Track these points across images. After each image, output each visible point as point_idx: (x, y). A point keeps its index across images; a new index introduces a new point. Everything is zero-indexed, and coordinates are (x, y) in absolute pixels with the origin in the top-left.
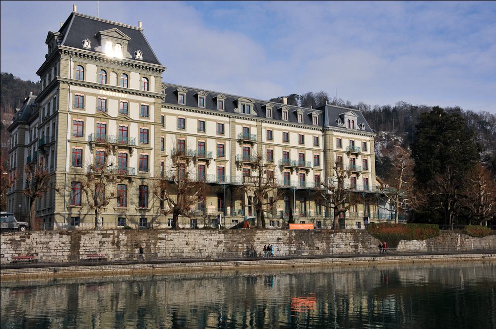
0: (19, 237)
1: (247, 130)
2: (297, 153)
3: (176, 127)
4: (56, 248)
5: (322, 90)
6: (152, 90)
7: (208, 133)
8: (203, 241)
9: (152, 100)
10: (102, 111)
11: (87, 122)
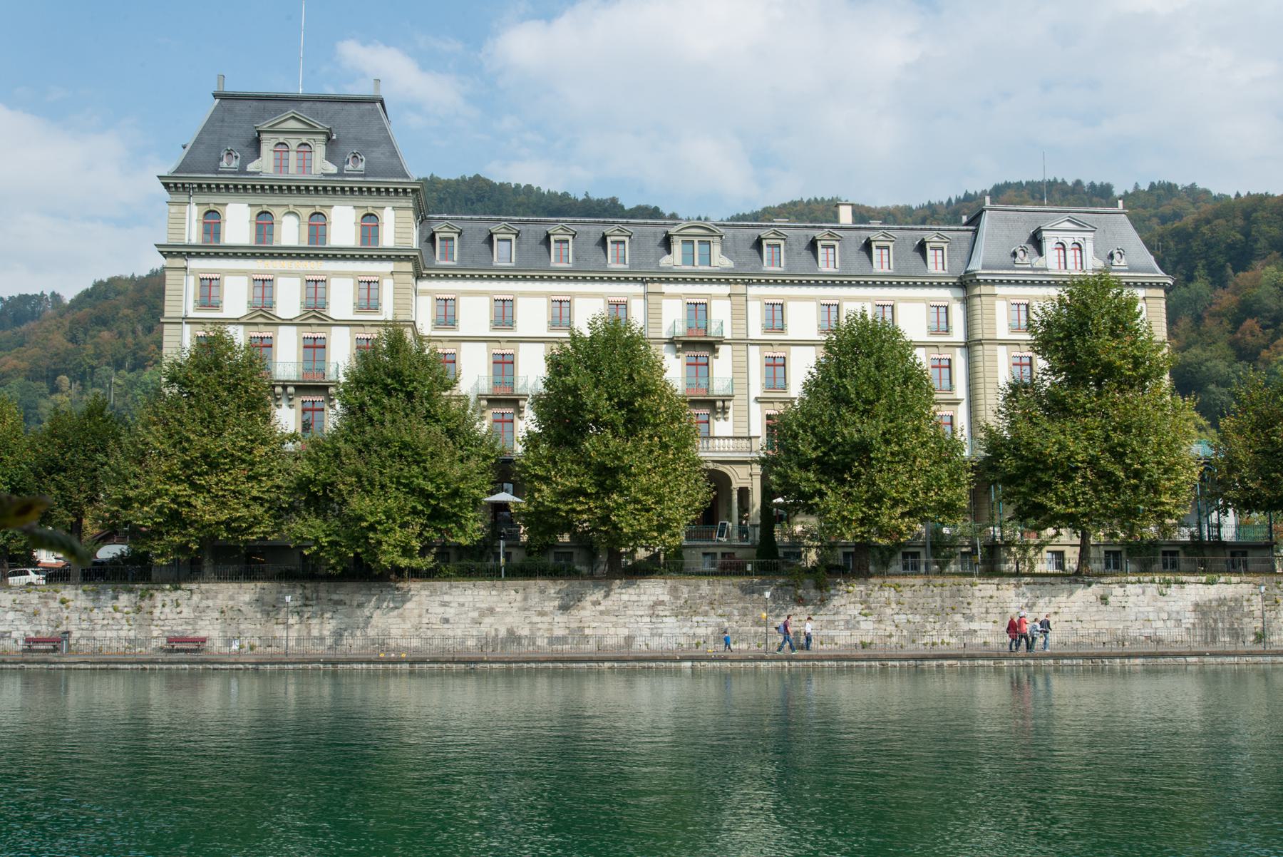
0: (37, 596)
1: (698, 309)
2: (295, 338)
3: (487, 324)
4: (105, 622)
5: (1112, 182)
6: (388, 239)
7: (521, 330)
8: (441, 610)
9: (388, 267)
10: (315, 313)
11: (279, 337)
